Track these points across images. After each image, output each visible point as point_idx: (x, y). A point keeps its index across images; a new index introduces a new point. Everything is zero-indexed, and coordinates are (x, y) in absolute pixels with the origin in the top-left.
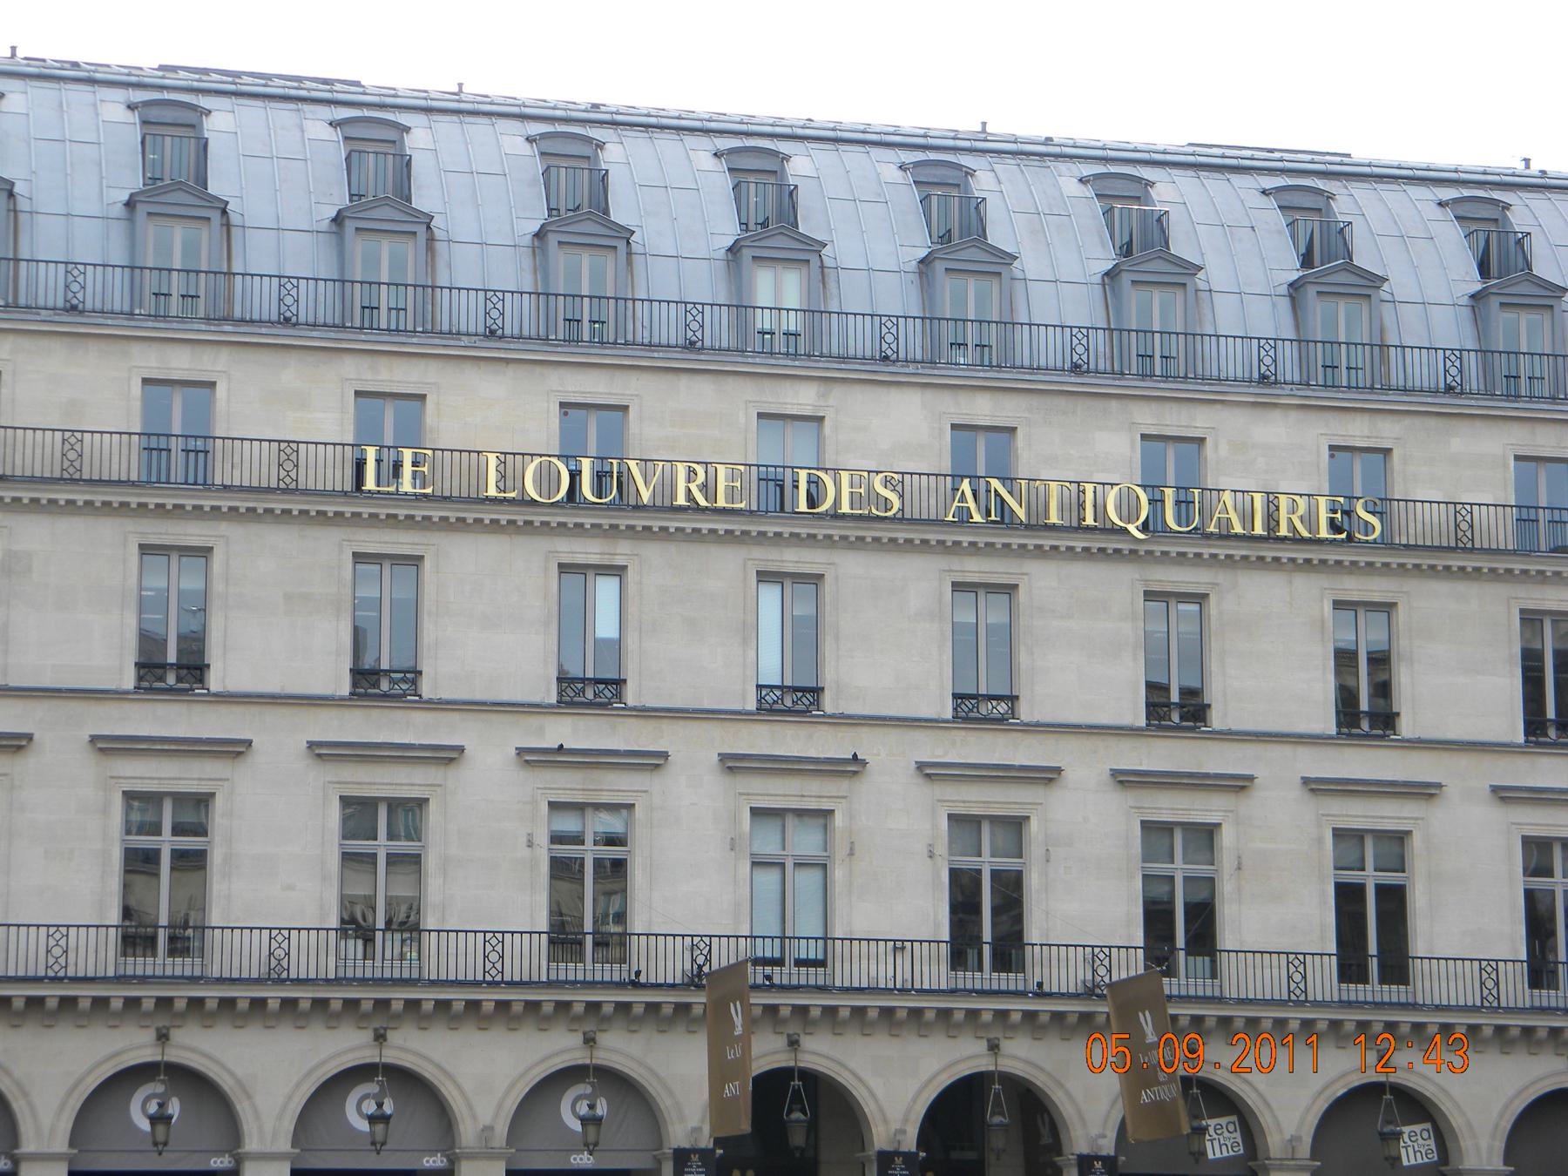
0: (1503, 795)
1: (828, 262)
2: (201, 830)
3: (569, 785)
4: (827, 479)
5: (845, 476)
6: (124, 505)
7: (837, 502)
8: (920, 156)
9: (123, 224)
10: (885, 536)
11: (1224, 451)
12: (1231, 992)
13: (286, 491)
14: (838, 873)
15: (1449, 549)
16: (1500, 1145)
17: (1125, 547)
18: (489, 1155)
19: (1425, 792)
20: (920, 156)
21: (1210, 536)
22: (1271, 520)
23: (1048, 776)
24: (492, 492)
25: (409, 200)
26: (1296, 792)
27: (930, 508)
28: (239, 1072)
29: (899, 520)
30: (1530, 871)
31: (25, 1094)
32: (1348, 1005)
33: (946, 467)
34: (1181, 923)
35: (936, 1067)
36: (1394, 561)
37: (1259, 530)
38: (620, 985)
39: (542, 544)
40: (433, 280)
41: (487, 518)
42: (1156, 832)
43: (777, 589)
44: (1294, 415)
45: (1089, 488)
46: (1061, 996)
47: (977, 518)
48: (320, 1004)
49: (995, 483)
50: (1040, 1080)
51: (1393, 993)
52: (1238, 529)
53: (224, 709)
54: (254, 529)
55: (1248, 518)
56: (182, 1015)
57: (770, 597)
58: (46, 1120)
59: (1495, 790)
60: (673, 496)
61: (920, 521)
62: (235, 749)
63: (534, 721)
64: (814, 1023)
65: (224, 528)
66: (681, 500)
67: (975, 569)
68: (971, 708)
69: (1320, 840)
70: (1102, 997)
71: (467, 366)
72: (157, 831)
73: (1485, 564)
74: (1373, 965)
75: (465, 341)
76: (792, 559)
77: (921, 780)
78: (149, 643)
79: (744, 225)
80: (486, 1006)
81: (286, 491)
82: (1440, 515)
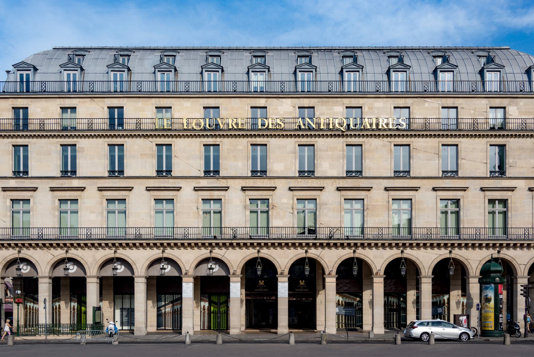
3: (207, 195)
14: (270, 213)
17: (340, 133)
19: (416, 189)
22: (377, 125)
23: (273, 189)
25: (403, 62)
28: (133, 259)
31: (135, 264)
33: (297, 116)
37: (374, 127)
45: (331, 119)
49: (308, 119)
52: (369, 127)
55: (371, 125)
58: (43, 269)
62: (130, 189)
64: (311, 247)
68: (255, 174)
76: (259, 140)
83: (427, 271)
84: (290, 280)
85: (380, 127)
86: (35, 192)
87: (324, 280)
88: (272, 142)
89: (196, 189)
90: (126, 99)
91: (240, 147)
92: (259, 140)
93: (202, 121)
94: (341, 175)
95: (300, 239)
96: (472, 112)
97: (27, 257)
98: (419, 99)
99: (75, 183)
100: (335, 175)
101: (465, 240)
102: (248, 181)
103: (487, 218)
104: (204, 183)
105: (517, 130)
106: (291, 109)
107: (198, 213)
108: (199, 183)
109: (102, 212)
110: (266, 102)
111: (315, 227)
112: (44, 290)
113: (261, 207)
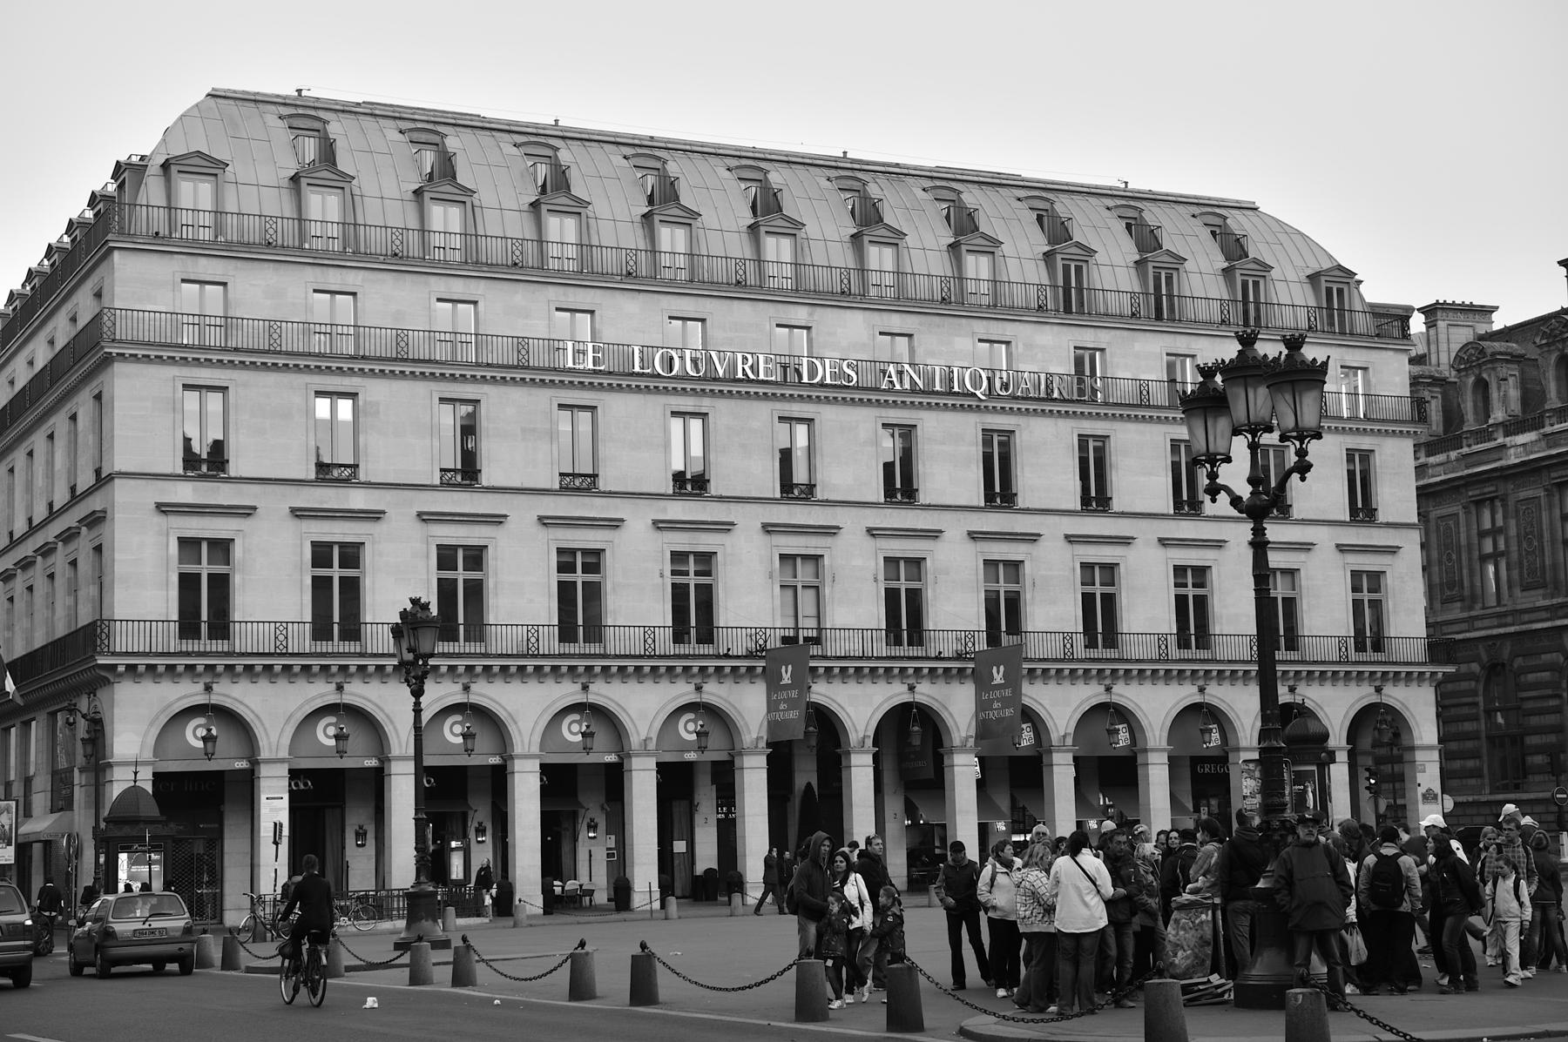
1: (356, 191)
2: (708, 573)
3: (682, 541)
4: (817, 363)
7: (824, 377)
8: (292, 111)
9: (414, 204)
10: (849, 396)
11: (1021, 349)
12: (610, 650)
13: (275, 352)
15: (396, 360)
16: (1165, 734)
17: (974, 404)
18: (648, 754)
19: (1125, 541)
20: (292, 111)
21: (1017, 398)
23: (934, 534)
24: (637, 369)
25: (334, 164)
26: (1062, 543)
27: (868, 381)
29: (857, 388)
30: (441, 566)
32: (679, 657)
34: (1004, 613)
36: (1110, 412)
37: (1043, 395)
38: (718, 657)
39: (433, 385)
40: (195, 202)
41: (634, 384)
42: (189, 545)
43: (328, 401)
46: (738, 657)
47: (898, 387)
48: (306, 669)
50: (936, 706)
51: (594, 648)
53: (490, 496)
57: (676, 425)
58: (274, 738)
59: (1160, 540)
60: (736, 372)
61: (539, 369)
63: (662, 503)
64: (352, 675)
65: (486, 388)
66: (740, 375)
70: (971, 659)
71: (617, 293)
72: (687, 573)
74: (204, 628)
75: (529, 271)
76: (797, 409)
80: (273, 667)
81: (275, 352)
84: (770, 760)
86: (1222, 551)
88: (828, 416)
89: (658, 525)
90: (483, 282)
92: (797, 409)
95: (188, 654)
97: (228, 703)
98: (1125, 333)
99: (357, 499)
101: (242, 655)
103: (778, 602)
105: (1395, 421)
108: (665, 510)
110: (811, 314)
111: (819, 629)
112: (1062, 777)
113: (804, 573)
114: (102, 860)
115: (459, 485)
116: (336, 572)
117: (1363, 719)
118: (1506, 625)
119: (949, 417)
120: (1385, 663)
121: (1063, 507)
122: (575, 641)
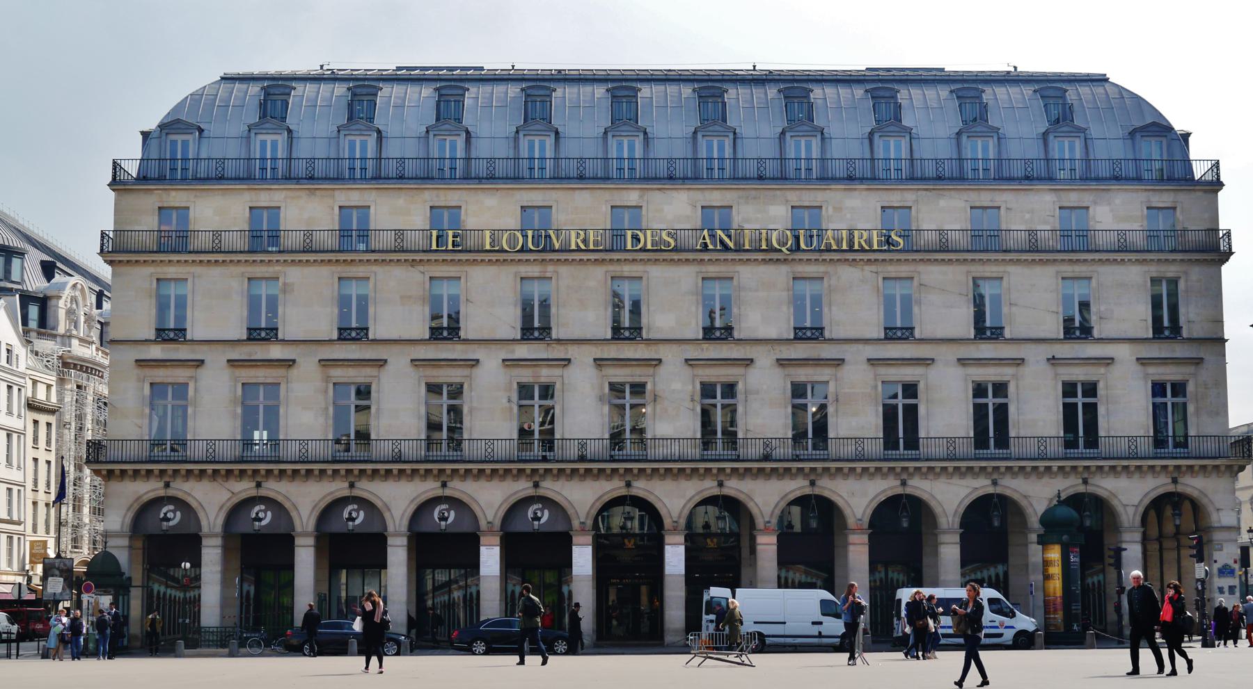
0: (962, 362)
3: (526, 375)
5: (649, 233)
6: (1115, 260)
8: (959, 86)
11: (830, 210)
23: (1020, 362)
24: (488, 247)
25: (987, 121)
26: (865, 366)
33: (699, 225)
35: (693, 493)
37: (845, 247)
39: (513, 269)
44: (864, 193)
45: (764, 232)
47: (711, 247)
49: (719, 232)
52: (834, 247)
54: (387, 268)
55: (839, 242)
56: (1003, 474)
58: (212, 518)
59: (959, 360)
63: (141, 347)
65: (374, 268)
66: (573, 247)
67: (712, 270)
69: (876, 387)
73: (228, 258)
74: (992, 442)
77: (687, 367)
78: (1068, 321)
79: (877, 121)
80: (675, 469)
82: (1113, 237)
83: (212, 518)
85: (856, 247)
87: (753, 539)
91: (592, 283)
93: (519, 234)
94: (785, 336)
96: (1027, 216)
100: (774, 335)
102: (606, 348)
104: (523, 351)
106: (688, 211)
107: (511, 409)
108: (513, 352)
109: (327, 409)
110: (641, 197)
114: (612, 597)
115: (1167, 338)
116: (1169, 399)
117: (1160, 506)
118: (1166, 423)
119: (763, 269)
120: (824, 460)
121: (868, 336)
122: (987, 448)
